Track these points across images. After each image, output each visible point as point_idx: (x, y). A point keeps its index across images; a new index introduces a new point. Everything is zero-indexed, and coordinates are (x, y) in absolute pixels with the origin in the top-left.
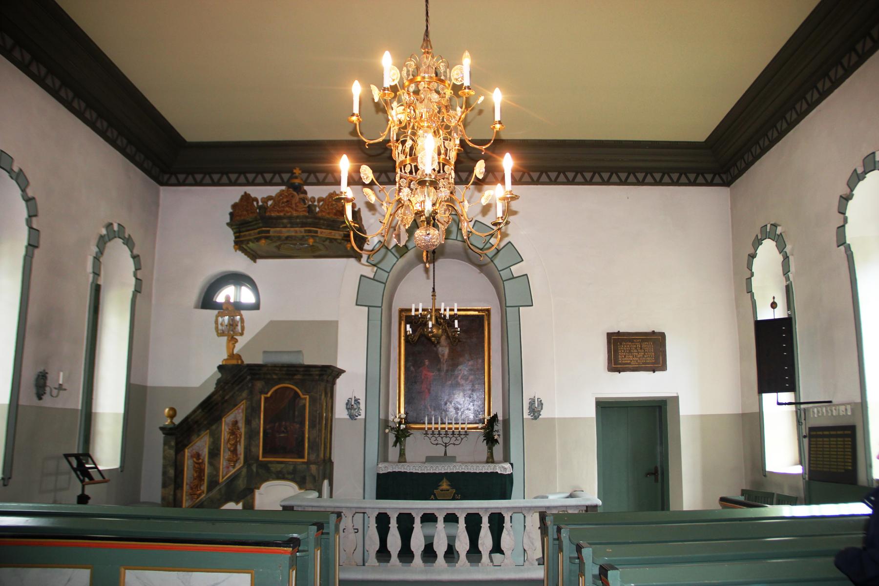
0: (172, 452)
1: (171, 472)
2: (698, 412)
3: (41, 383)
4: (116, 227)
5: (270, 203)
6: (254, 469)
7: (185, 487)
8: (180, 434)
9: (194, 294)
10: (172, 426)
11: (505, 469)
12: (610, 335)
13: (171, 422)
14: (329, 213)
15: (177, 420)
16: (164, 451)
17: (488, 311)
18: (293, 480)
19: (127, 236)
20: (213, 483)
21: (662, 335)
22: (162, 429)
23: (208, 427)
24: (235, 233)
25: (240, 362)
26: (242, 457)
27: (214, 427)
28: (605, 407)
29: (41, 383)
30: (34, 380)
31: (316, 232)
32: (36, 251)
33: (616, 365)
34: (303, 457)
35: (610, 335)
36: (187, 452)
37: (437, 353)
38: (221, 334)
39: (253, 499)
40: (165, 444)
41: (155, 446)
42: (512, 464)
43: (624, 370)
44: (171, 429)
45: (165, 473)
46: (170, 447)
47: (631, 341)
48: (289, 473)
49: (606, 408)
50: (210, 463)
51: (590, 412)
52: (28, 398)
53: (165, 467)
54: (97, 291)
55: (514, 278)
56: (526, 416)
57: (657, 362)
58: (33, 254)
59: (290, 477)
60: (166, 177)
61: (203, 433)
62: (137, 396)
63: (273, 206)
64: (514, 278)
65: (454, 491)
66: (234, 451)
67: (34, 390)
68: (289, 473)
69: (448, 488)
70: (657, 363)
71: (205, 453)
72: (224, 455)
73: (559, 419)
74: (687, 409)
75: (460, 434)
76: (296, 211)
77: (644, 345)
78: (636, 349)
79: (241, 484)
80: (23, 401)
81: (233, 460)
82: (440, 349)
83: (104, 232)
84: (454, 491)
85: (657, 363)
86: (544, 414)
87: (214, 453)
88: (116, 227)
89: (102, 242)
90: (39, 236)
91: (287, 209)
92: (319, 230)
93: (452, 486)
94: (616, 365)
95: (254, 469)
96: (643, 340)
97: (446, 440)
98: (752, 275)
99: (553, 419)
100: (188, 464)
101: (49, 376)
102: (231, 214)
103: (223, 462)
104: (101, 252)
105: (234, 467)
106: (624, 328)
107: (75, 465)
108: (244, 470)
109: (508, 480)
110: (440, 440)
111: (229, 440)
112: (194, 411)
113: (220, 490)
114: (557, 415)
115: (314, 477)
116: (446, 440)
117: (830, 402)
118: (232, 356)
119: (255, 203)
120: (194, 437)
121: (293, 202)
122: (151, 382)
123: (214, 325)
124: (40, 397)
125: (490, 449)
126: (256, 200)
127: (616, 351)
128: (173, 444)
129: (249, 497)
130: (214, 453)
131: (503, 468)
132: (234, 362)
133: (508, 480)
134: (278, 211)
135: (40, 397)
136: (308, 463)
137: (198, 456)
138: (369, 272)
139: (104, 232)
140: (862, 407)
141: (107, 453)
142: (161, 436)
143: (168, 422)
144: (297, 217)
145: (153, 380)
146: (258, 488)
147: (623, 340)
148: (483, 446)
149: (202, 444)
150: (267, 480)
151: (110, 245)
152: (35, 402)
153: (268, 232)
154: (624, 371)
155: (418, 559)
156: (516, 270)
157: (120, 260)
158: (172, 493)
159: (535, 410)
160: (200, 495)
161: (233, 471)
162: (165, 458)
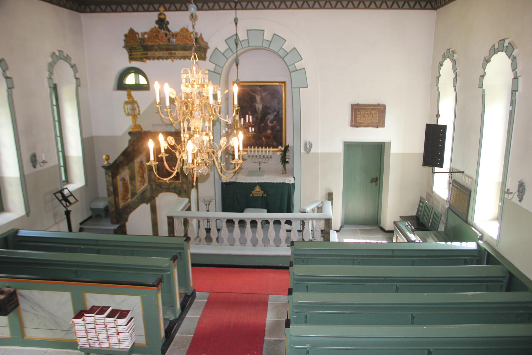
0: (110, 179)
1: (111, 189)
2: (401, 152)
3: (34, 160)
4: (57, 53)
5: (146, 36)
6: (154, 187)
7: (120, 196)
8: (113, 169)
9: (112, 81)
10: (108, 165)
11: (290, 181)
12: (353, 106)
13: (108, 163)
14: (182, 42)
15: (111, 161)
16: (106, 178)
17: (284, 83)
18: (175, 192)
19: (65, 55)
20: (134, 194)
21: (384, 106)
22: (104, 167)
23: (127, 164)
24: (128, 52)
25: (140, 130)
26: (147, 180)
27: (130, 165)
28: (349, 146)
29: (34, 160)
30: (29, 161)
31: (175, 54)
32: (13, 90)
33: (355, 123)
34: (179, 180)
35: (353, 106)
36: (118, 178)
37: (255, 107)
38: (128, 114)
39: (155, 201)
40: (106, 174)
41: (102, 177)
42: (294, 178)
43: (360, 126)
44: (108, 167)
45: (108, 189)
46: (109, 176)
47: (365, 109)
48: (172, 189)
49: (350, 147)
50: (131, 184)
51: (340, 149)
52: (29, 169)
53: (108, 186)
54: (55, 88)
55: (297, 70)
56: (303, 151)
57: (379, 122)
58: (12, 92)
59: (173, 191)
60: (83, 7)
61: (125, 168)
62: (88, 144)
63: (149, 38)
64: (297, 70)
65: (263, 192)
66: (143, 177)
67: (31, 165)
68: (172, 189)
69: (259, 190)
70: (380, 123)
71: (127, 178)
72: (138, 179)
73: (321, 153)
74: (394, 149)
75: (267, 157)
76: (162, 41)
77: (373, 112)
78: (367, 114)
79: (148, 194)
80: (26, 172)
81: (143, 182)
82: (257, 105)
83: (50, 60)
84: (263, 192)
85: (380, 123)
86: (313, 150)
87: (132, 178)
88: (57, 53)
89: (51, 66)
90: (12, 81)
91: (156, 40)
92: (177, 52)
93: (262, 189)
94: (355, 123)
95: (154, 187)
96: (372, 109)
97: (260, 160)
98: (440, 76)
99: (318, 153)
100: (120, 184)
101: (37, 155)
102: (125, 40)
103: (138, 183)
104: (51, 73)
105: (143, 185)
106: (362, 101)
107: (61, 198)
108: (149, 187)
109: (289, 189)
110: (256, 159)
111: (139, 171)
112: (119, 157)
113: (137, 198)
114: (320, 151)
115: (186, 191)
116: (260, 160)
117: (463, 172)
118: (136, 126)
119: (137, 36)
120: (121, 170)
121: (160, 36)
122: (95, 133)
123: (123, 110)
124: (34, 167)
125: (284, 166)
126: (138, 34)
127: (356, 116)
128: (110, 174)
129: (153, 201)
130: (132, 178)
131: (289, 180)
132: (137, 130)
133: (289, 189)
134: (152, 42)
135: (34, 167)
136: (182, 183)
137: (124, 180)
138: (212, 67)
139: (50, 60)
140: (476, 183)
141: (78, 181)
142: (103, 171)
143: (106, 163)
144: (163, 45)
145: (96, 132)
146: (157, 196)
147: (362, 109)
148: (281, 166)
149: (125, 173)
150: (161, 192)
151: (56, 67)
152: (34, 170)
153: (147, 54)
154: (360, 127)
155: (237, 242)
156: (298, 65)
157: (65, 75)
158: (113, 199)
159: (308, 147)
160: (127, 200)
161: (143, 187)
162: (107, 181)
